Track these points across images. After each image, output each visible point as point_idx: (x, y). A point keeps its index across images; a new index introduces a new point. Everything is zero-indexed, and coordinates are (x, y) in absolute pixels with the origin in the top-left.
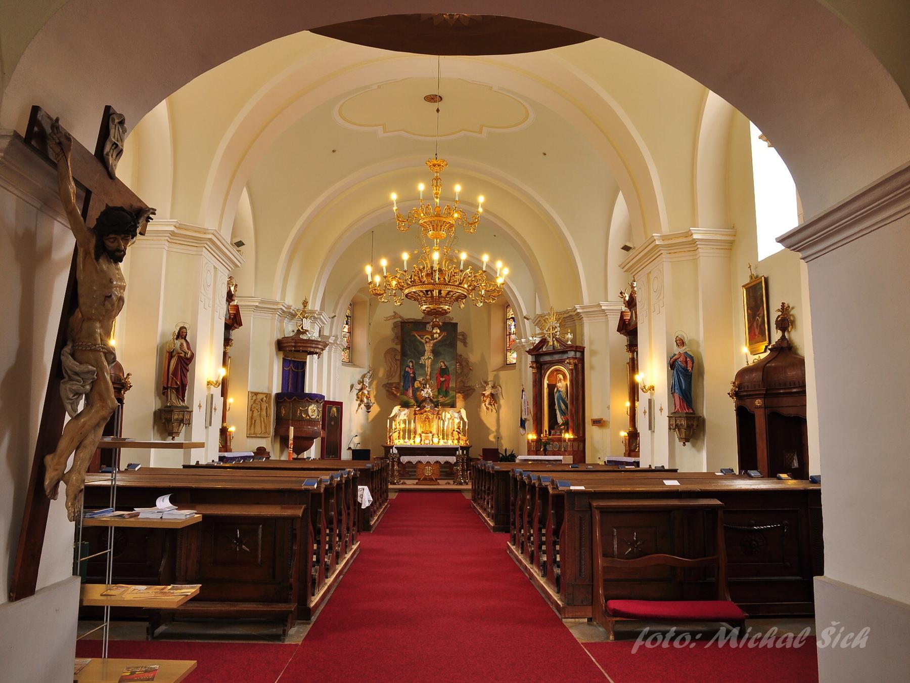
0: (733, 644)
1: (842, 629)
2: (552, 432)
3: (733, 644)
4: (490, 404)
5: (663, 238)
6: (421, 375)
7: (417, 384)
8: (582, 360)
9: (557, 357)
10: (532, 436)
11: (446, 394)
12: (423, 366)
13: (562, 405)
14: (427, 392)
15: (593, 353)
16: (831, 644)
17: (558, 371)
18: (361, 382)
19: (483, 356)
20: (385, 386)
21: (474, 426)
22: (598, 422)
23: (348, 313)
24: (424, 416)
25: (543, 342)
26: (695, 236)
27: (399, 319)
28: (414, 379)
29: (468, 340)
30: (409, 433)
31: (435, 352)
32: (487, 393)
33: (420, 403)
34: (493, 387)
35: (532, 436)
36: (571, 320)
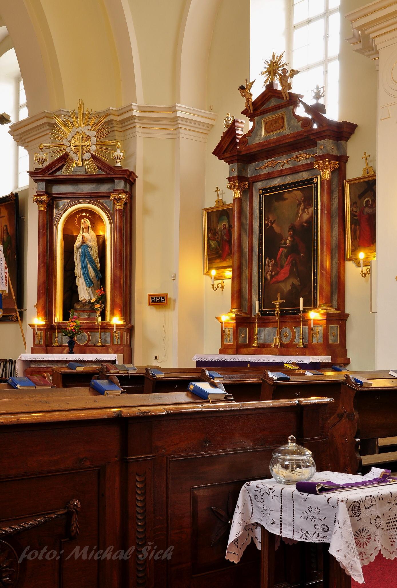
0: (84, 557)
1: (155, 547)
3: (84, 557)
5: (141, 109)
9: (87, 188)
10: (39, 321)
15: (150, 188)
17: (95, 218)
22: (159, 301)
25: (64, 159)
26: (179, 114)
35: (39, 321)
36: (113, 125)
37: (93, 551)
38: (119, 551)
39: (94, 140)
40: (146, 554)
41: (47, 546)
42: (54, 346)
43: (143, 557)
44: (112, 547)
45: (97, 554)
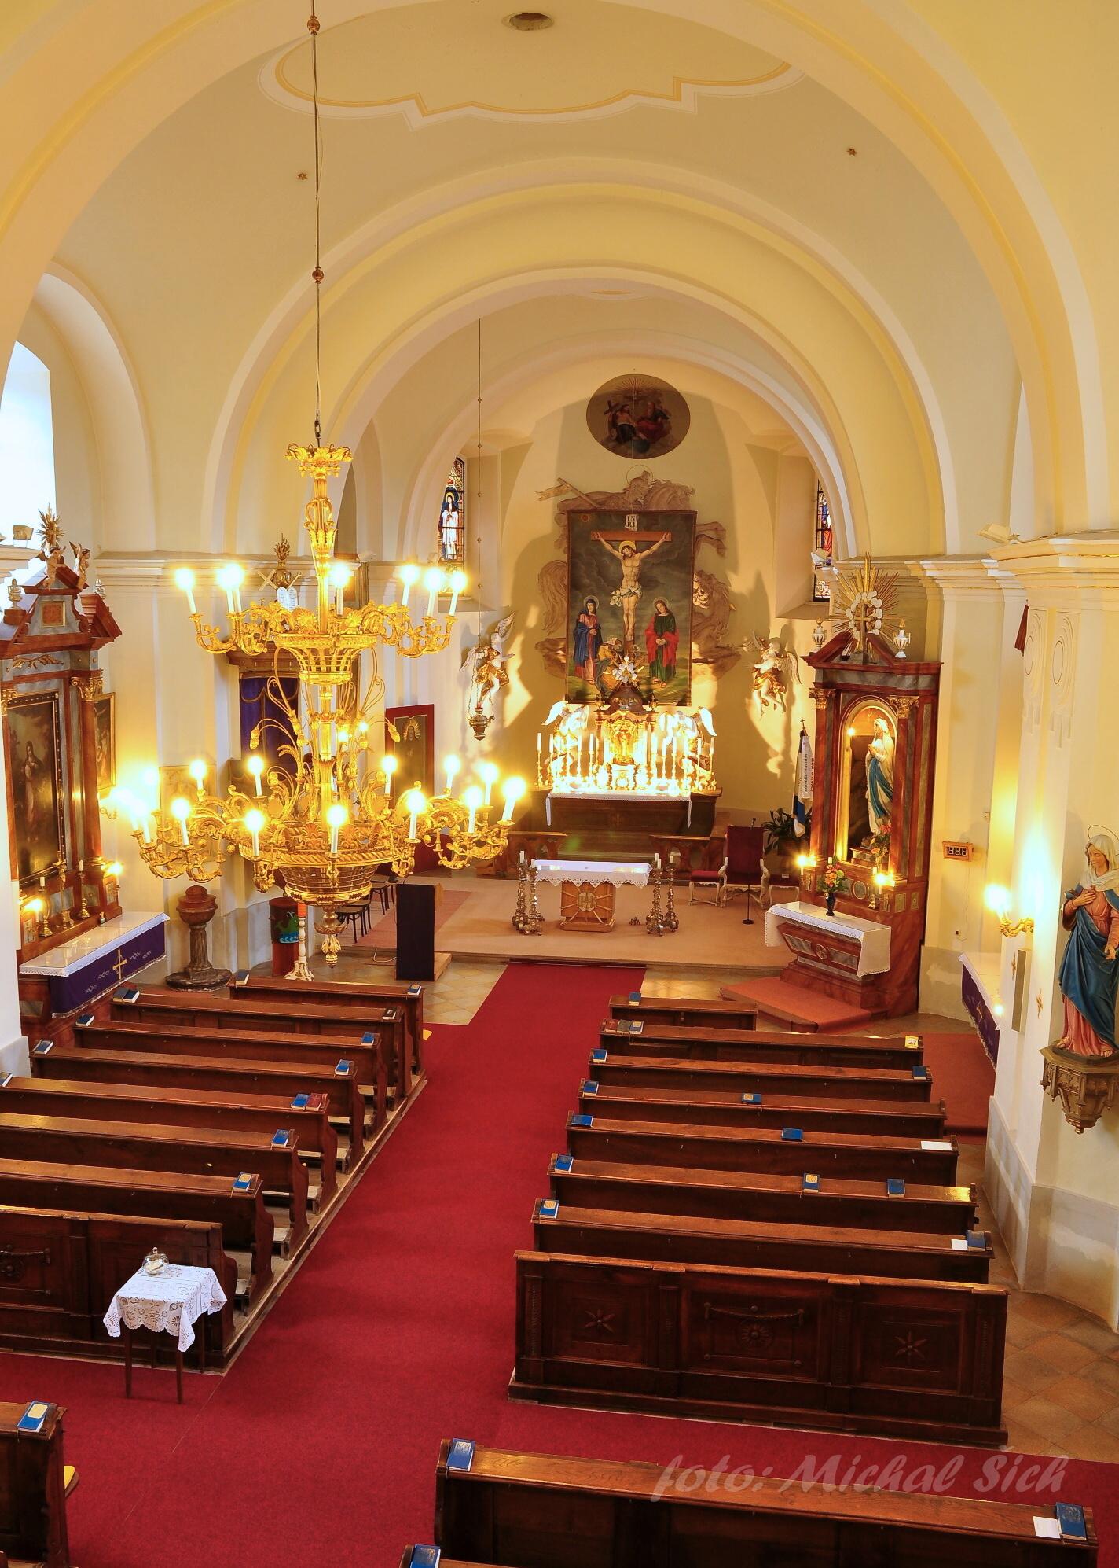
2: (855, 853)
4: (771, 692)
6: (611, 632)
7: (604, 653)
8: (933, 694)
11: (669, 674)
12: (616, 612)
13: (884, 798)
14: (624, 672)
16: (999, 1485)
18: (485, 643)
19: (759, 580)
20: (541, 645)
21: (733, 735)
22: (958, 852)
23: (454, 479)
24: (617, 726)
27: (571, 495)
28: (598, 641)
29: (727, 543)
30: (587, 761)
31: (645, 580)
32: (765, 667)
33: (612, 697)
34: (778, 655)
37: (853, 1470)
38: (920, 1470)
39: (879, 613)
40: (994, 1478)
41: (728, 1457)
42: (446, 871)
43: (986, 1483)
44: (680, 1458)
45: (864, 1475)
